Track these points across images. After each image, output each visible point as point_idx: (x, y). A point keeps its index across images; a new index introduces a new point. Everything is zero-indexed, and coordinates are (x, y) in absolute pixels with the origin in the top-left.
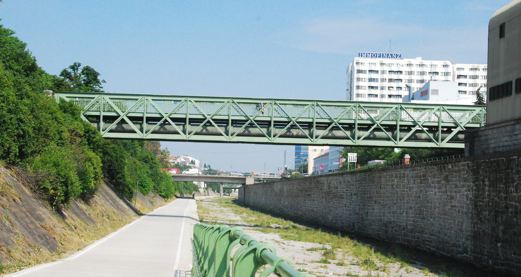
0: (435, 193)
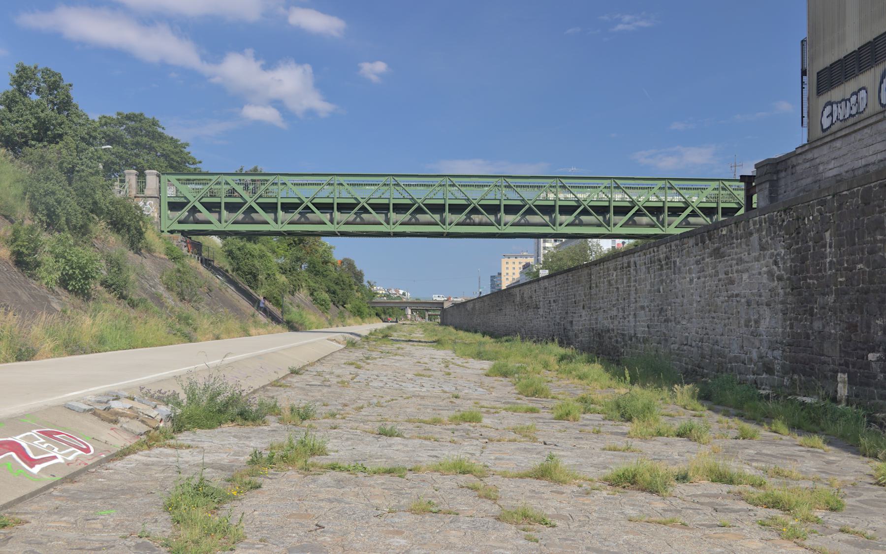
0: (691, 281)
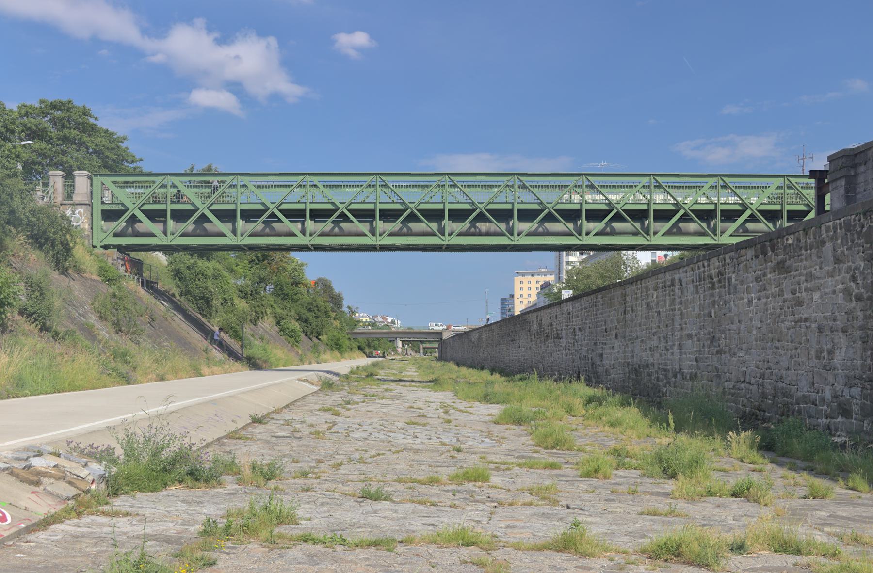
0: (750, 302)
